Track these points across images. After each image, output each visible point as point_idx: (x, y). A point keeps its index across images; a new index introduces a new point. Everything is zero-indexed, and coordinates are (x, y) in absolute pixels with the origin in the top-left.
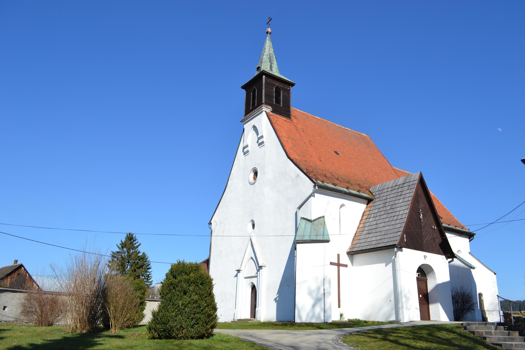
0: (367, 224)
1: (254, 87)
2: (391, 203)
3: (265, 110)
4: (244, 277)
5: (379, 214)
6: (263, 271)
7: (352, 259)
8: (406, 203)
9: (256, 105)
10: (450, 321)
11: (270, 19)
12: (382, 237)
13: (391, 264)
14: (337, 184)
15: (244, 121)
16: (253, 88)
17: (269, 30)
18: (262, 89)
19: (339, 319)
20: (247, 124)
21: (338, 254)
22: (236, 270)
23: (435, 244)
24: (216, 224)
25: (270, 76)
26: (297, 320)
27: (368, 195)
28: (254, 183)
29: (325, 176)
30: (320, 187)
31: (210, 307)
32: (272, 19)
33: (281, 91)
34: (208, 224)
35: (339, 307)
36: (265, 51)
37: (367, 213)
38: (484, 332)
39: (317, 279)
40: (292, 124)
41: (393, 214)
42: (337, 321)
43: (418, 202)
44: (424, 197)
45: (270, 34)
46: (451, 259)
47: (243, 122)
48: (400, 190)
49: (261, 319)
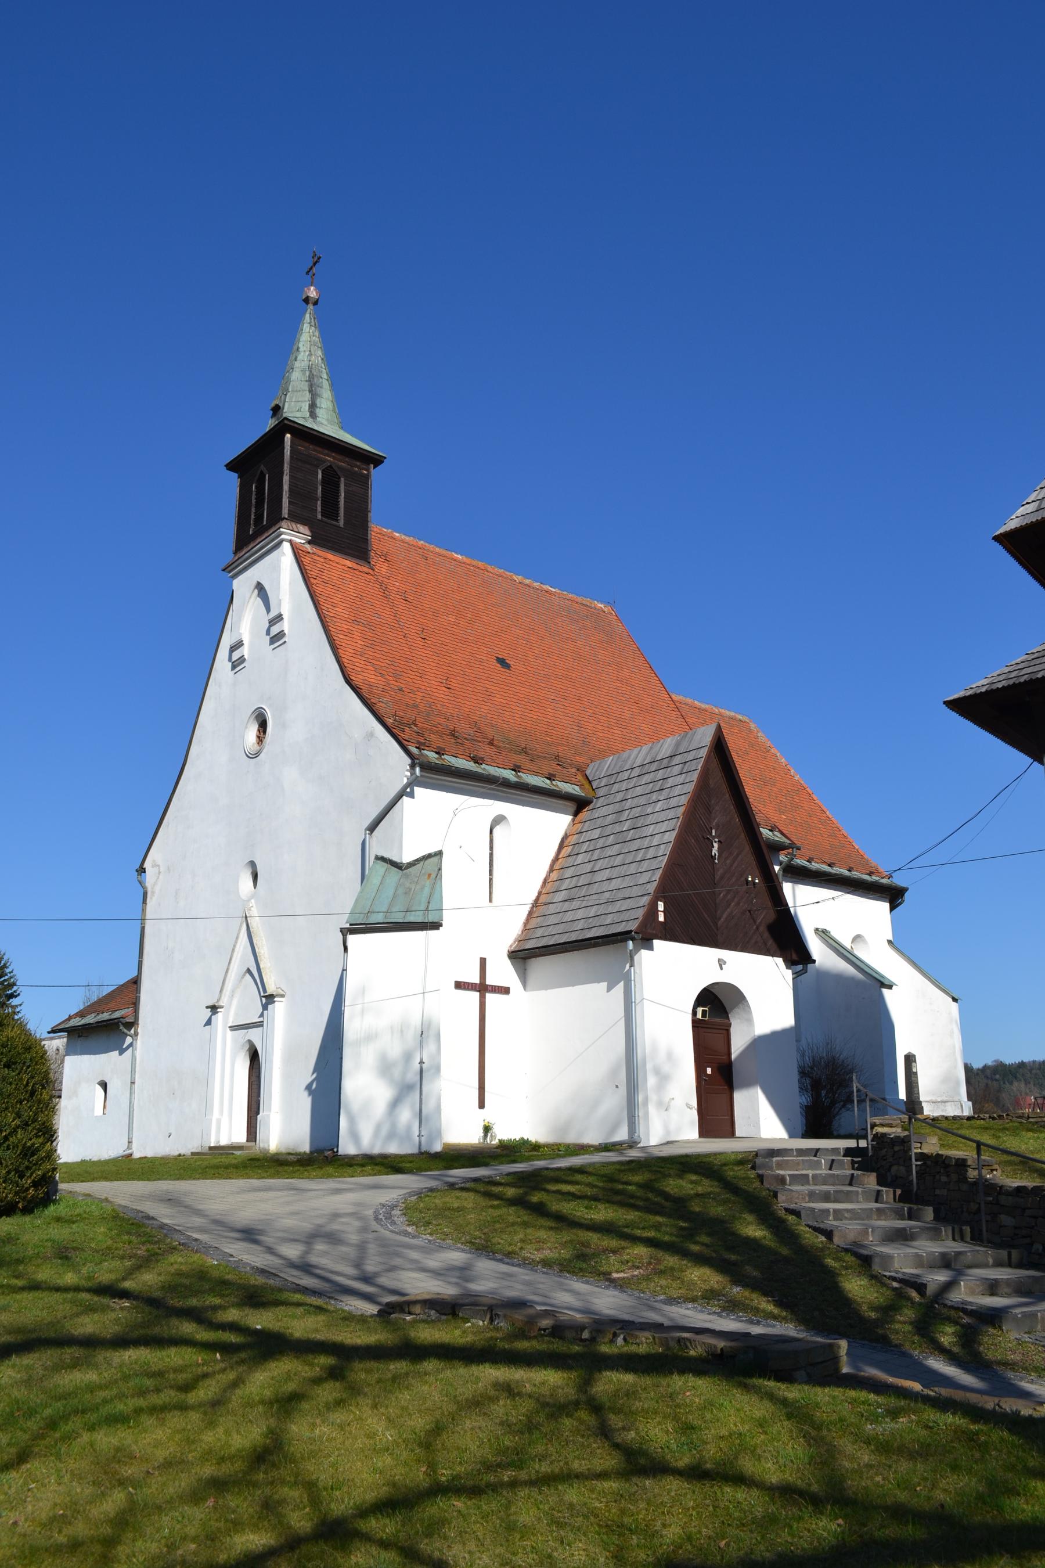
0: (569, 873)
1: (262, 467)
2: (636, 812)
3: (289, 538)
4: (230, 1027)
5: (600, 843)
6: (279, 1007)
7: (525, 970)
8: (671, 814)
9: (265, 523)
10: (791, 1136)
11: (316, 259)
12: (602, 910)
13: (622, 983)
14: (482, 759)
15: (233, 569)
16: (259, 472)
17: (312, 292)
18: (283, 473)
19: (479, 1140)
20: (241, 577)
21: (481, 958)
22: (207, 1007)
23: (755, 927)
24: (157, 872)
25: (305, 435)
26: (347, 1147)
27: (577, 788)
28: (257, 755)
29: (453, 734)
30: (428, 767)
31: (30, 1128)
32: (321, 260)
33: (342, 479)
34: (137, 871)
35: (482, 1105)
36: (298, 359)
37: (573, 840)
38: (789, 1175)
39: (402, 1032)
40: (371, 577)
41: (636, 844)
42: (472, 1146)
43: (709, 810)
44: (728, 795)
45: (316, 303)
46: (800, 967)
47: (230, 572)
48: (660, 774)
49: (269, 1146)
